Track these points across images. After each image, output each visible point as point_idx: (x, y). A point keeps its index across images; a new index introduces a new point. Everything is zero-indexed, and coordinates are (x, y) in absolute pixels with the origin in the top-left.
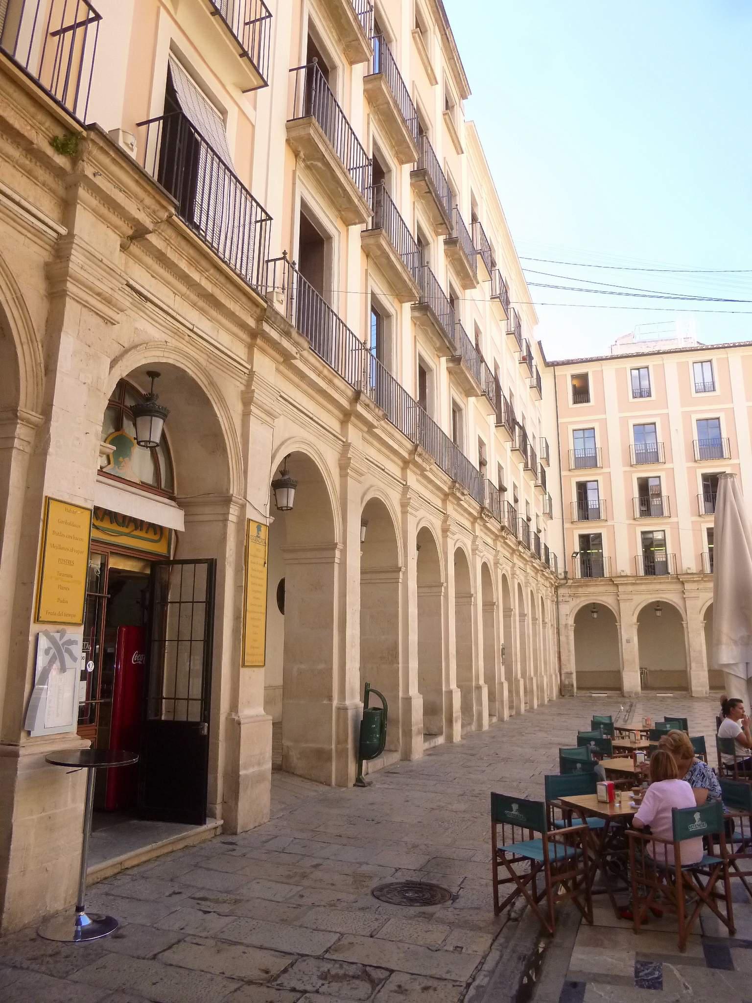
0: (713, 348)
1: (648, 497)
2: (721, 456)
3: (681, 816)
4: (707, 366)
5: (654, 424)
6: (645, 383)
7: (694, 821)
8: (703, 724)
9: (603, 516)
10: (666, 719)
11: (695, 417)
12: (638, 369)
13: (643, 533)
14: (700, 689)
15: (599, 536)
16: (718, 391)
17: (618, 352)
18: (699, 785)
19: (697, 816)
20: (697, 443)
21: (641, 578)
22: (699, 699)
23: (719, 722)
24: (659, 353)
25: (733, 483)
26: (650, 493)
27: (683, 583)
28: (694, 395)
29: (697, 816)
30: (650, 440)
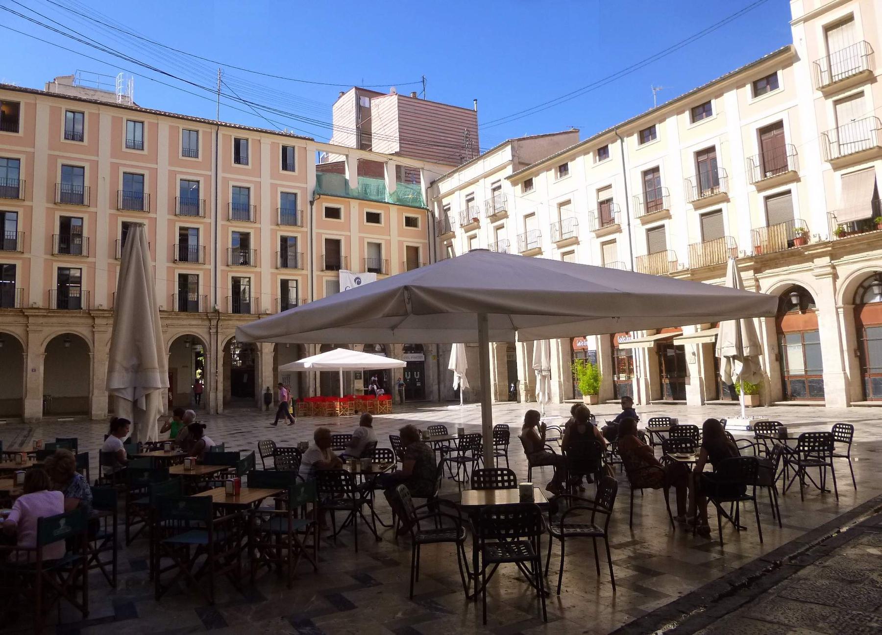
0: (146, 112)
1: (68, 237)
2: (141, 209)
3: (46, 525)
4: (139, 126)
5: (83, 168)
6: (78, 127)
7: (59, 526)
8: (94, 442)
9: (19, 248)
10: (58, 440)
11: (122, 170)
12: (74, 112)
13: (59, 269)
14: (100, 412)
15: (13, 267)
16: (145, 152)
17: (56, 90)
18: (72, 495)
19: (62, 522)
20: (121, 193)
21: (53, 311)
22: (98, 422)
23: (106, 437)
24: (95, 102)
25: (141, 232)
26: (71, 233)
27: (93, 318)
28: (124, 149)
29: (62, 522)
30: (77, 183)
